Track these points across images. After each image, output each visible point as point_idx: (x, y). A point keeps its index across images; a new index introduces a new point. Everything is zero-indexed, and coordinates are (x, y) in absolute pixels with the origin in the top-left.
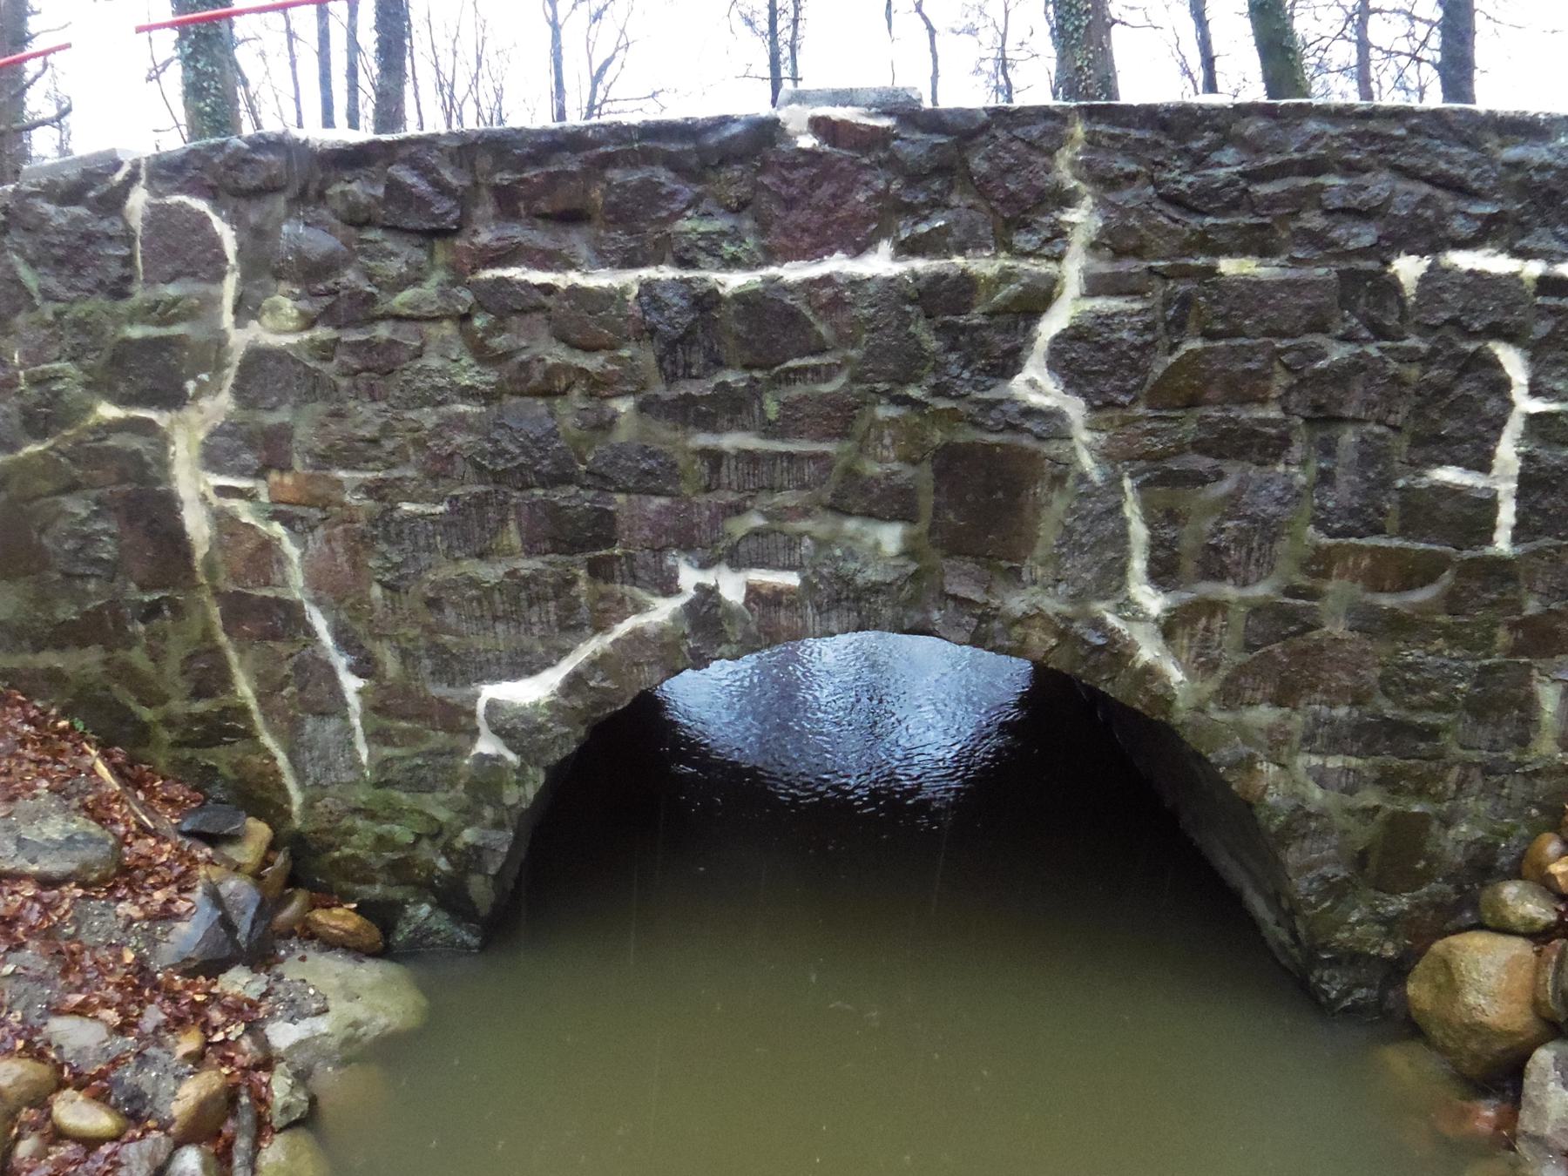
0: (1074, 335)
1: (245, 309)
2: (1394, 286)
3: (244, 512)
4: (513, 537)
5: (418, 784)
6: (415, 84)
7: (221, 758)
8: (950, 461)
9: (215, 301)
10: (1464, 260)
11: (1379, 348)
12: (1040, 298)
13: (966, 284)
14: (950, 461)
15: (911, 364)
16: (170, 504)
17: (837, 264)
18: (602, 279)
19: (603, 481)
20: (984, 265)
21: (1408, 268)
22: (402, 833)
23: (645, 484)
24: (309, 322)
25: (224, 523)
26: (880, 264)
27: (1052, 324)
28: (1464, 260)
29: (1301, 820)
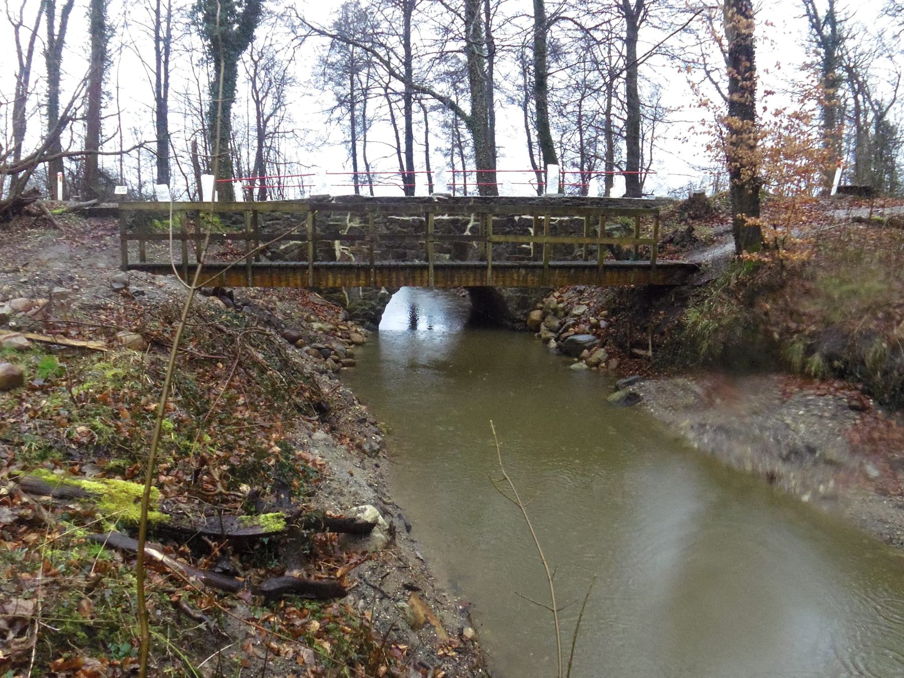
0: (472, 227)
1: (350, 221)
2: (514, 221)
3: (346, 252)
4: (390, 256)
5: (371, 299)
6: (19, 47)
7: (335, 295)
8: (456, 245)
9: (345, 219)
10: (524, 217)
11: (29, 339)
12: (468, 222)
13: (458, 220)
14: (456, 245)
15: (450, 231)
16: (334, 250)
17: (440, 217)
18: (407, 218)
19: (405, 248)
20: (460, 218)
21: (516, 218)
22: (367, 308)
23: (412, 248)
24: (361, 223)
25: (342, 254)
26: (446, 217)
27: (469, 226)
28: (524, 217)
29: (510, 299)
